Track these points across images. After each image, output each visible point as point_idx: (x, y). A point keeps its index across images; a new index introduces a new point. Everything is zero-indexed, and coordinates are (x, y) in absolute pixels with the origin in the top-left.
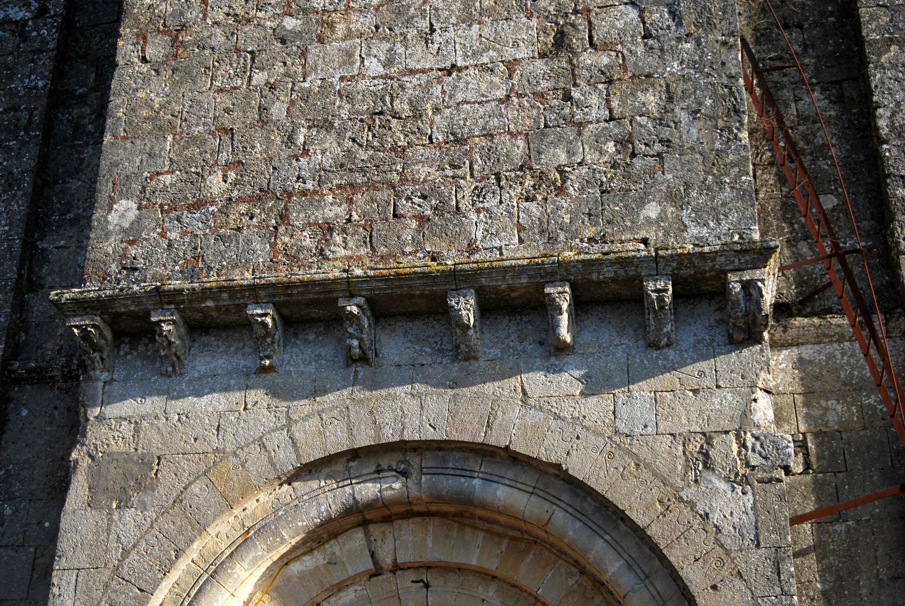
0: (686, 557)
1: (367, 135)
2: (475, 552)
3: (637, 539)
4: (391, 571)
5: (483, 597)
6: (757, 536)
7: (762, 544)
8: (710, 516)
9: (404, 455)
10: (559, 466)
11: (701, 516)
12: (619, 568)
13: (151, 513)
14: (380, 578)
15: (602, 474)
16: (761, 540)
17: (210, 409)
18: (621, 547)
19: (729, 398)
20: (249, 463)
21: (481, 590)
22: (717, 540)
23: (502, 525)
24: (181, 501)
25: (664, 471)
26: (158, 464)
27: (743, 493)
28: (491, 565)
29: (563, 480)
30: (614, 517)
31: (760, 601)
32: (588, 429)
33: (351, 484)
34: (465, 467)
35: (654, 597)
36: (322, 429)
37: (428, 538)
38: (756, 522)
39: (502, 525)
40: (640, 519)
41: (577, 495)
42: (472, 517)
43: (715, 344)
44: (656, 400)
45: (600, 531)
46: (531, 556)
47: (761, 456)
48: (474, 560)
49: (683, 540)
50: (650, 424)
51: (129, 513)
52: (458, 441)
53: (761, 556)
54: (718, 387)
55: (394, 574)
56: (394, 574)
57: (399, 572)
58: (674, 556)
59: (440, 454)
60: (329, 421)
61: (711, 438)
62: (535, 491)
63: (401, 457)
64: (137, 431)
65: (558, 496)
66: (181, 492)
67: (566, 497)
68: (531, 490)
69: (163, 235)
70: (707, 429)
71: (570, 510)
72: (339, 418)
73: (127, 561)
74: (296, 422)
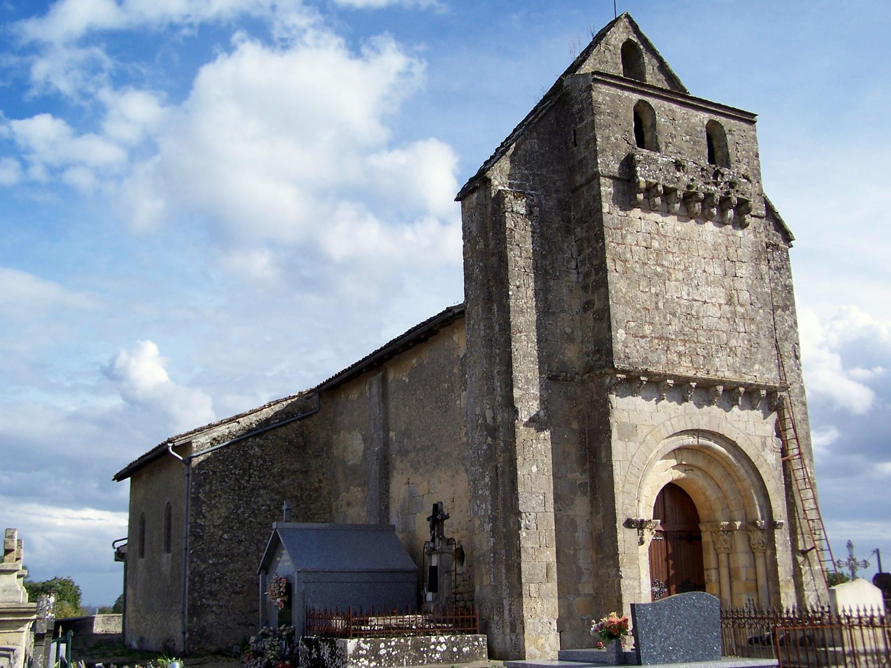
1: (686, 322)
2: (700, 462)
13: (638, 444)
51: (631, 443)
69: (635, 346)
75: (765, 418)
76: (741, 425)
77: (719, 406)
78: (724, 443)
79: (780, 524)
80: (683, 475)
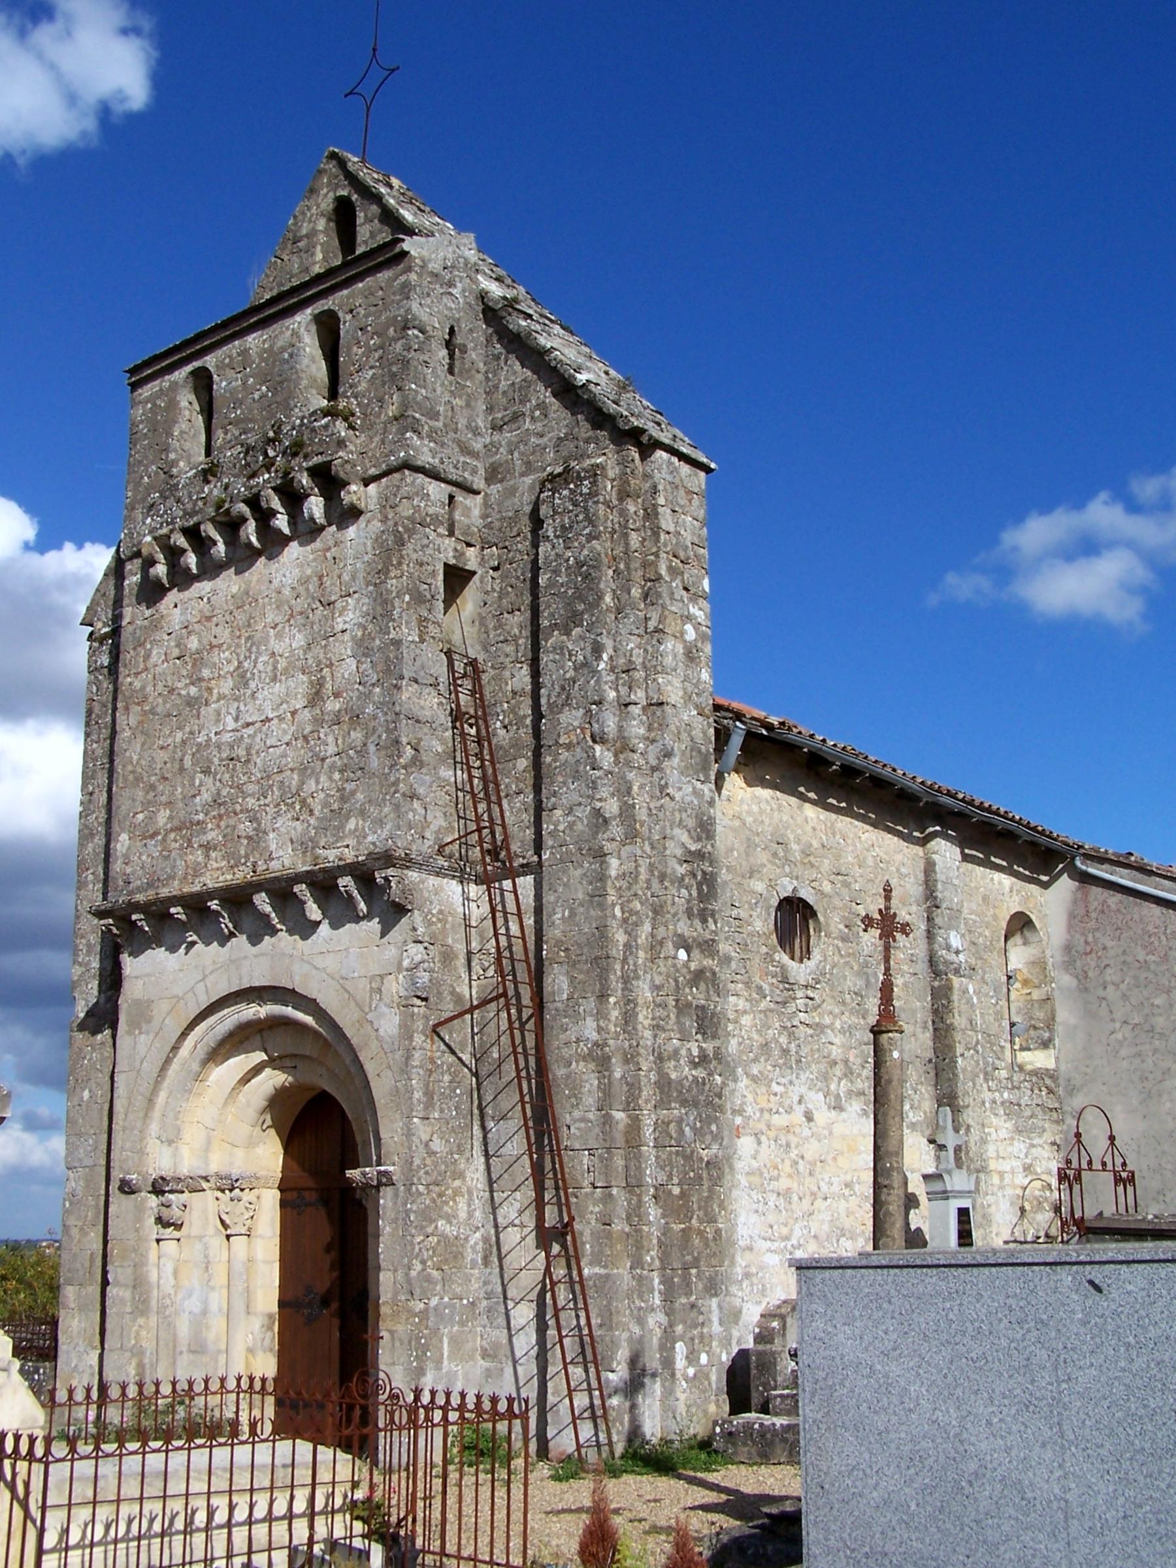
13: (152, 1036)
75: (383, 934)
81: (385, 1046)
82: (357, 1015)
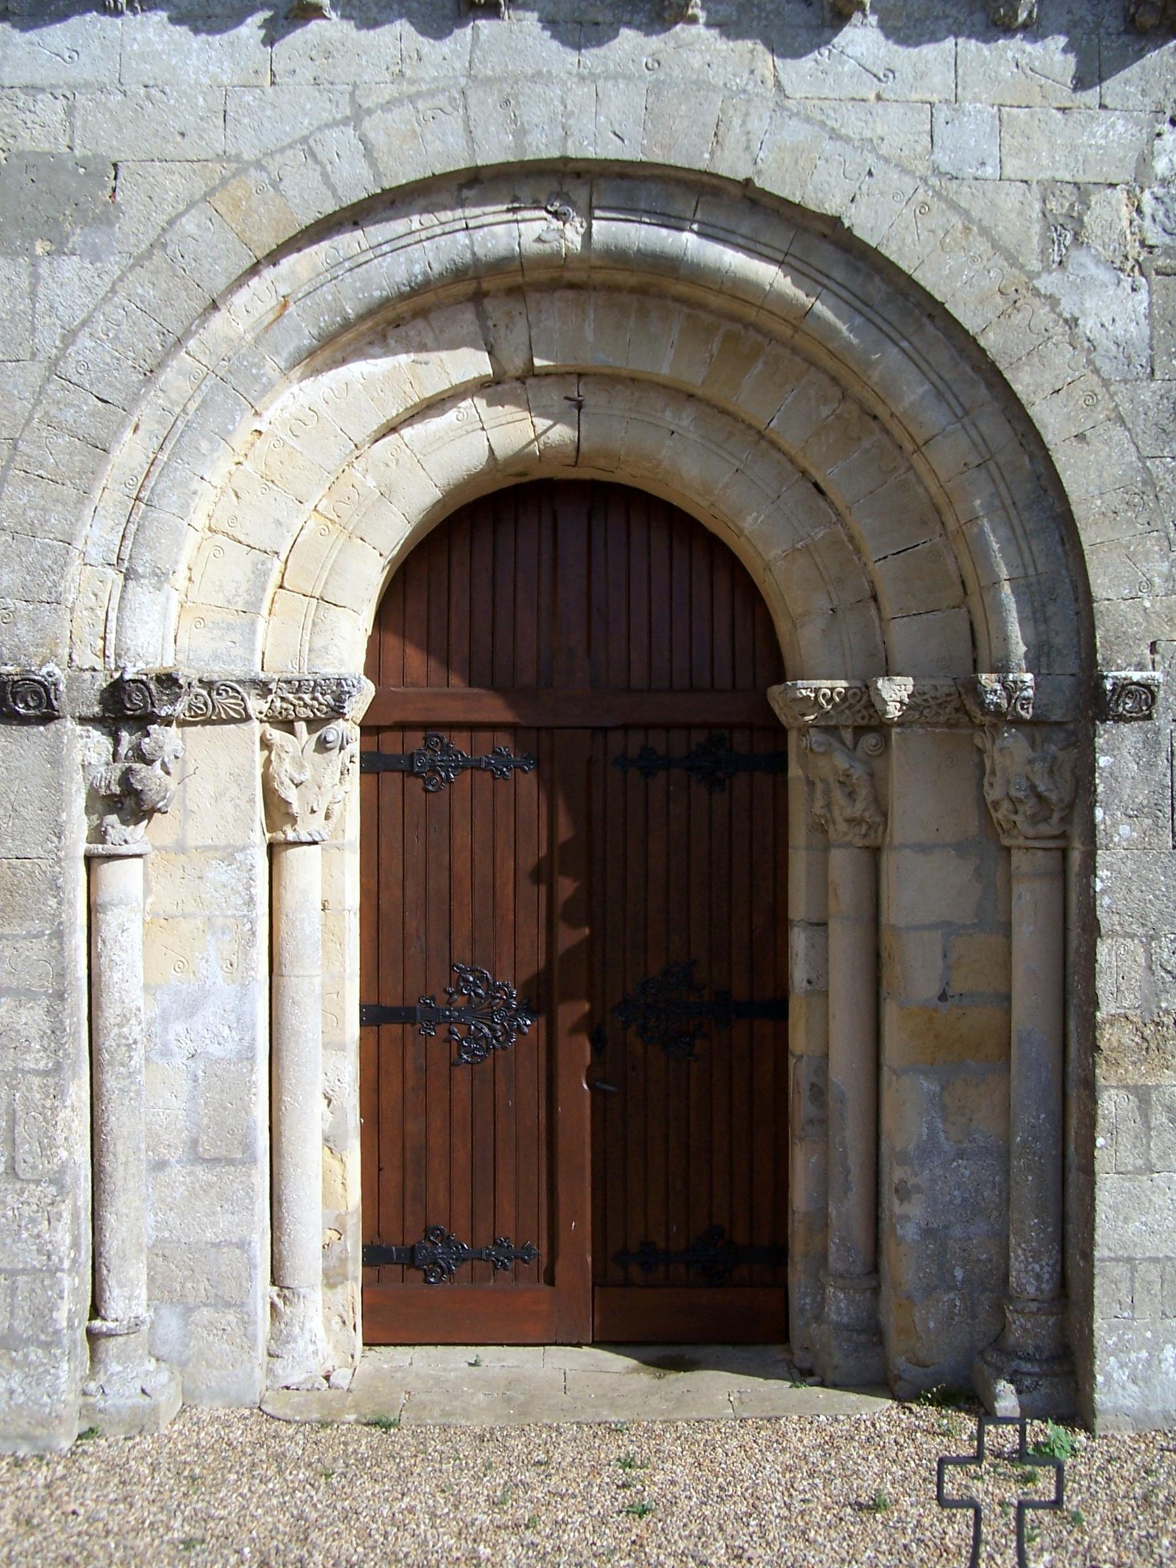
0: (1039, 386)
2: (666, 356)
3: (953, 350)
4: (518, 379)
5: (672, 428)
6: (1151, 359)
7: (1158, 375)
8: (1080, 322)
9: (560, 184)
10: (836, 221)
11: (1066, 321)
12: (923, 397)
13: (113, 265)
14: (500, 388)
15: (909, 241)
16: (1156, 368)
17: (206, 81)
18: (927, 362)
19: (1120, 128)
20: (286, 182)
21: (668, 415)
22: (1090, 362)
23: (712, 312)
24: (164, 246)
25: (1008, 241)
26: (115, 178)
27: (1134, 290)
28: (694, 377)
29: (835, 243)
30: (917, 312)
31: (1148, 464)
32: (887, 161)
33: (467, 228)
34: (668, 211)
35: (974, 444)
36: (418, 129)
37: (586, 326)
38: (1151, 339)
39: (712, 312)
40: (970, 321)
41: (858, 270)
42: (662, 295)
43: (1102, 30)
44: (1000, 120)
45: (893, 334)
46: (759, 366)
47: (1165, 230)
48: (664, 369)
49: (1036, 359)
50: (989, 161)
51: (69, 266)
52: (664, 165)
53: (1154, 393)
54: (1102, 106)
55: (524, 383)
56: (524, 383)
57: (530, 381)
58: (1022, 383)
59: (625, 184)
60: (429, 113)
61: (1088, 194)
62: (789, 259)
63: (555, 186)
64: (70, 112)
65: (825, 271)
66: (163, 229)
67: (839, 274)
68: (780, 257)
70: (1081, 178)
71: (845, 294)
72: (449, 109)
73: (72, 350)
74: (369, 112)
75: (1081, 83)
76: (896, 128)
77: (728, 28)
78: (780, 238)
79: (1123, 688)
80: (561, 433)
81: (1106, 368)
82: (996, 274)
